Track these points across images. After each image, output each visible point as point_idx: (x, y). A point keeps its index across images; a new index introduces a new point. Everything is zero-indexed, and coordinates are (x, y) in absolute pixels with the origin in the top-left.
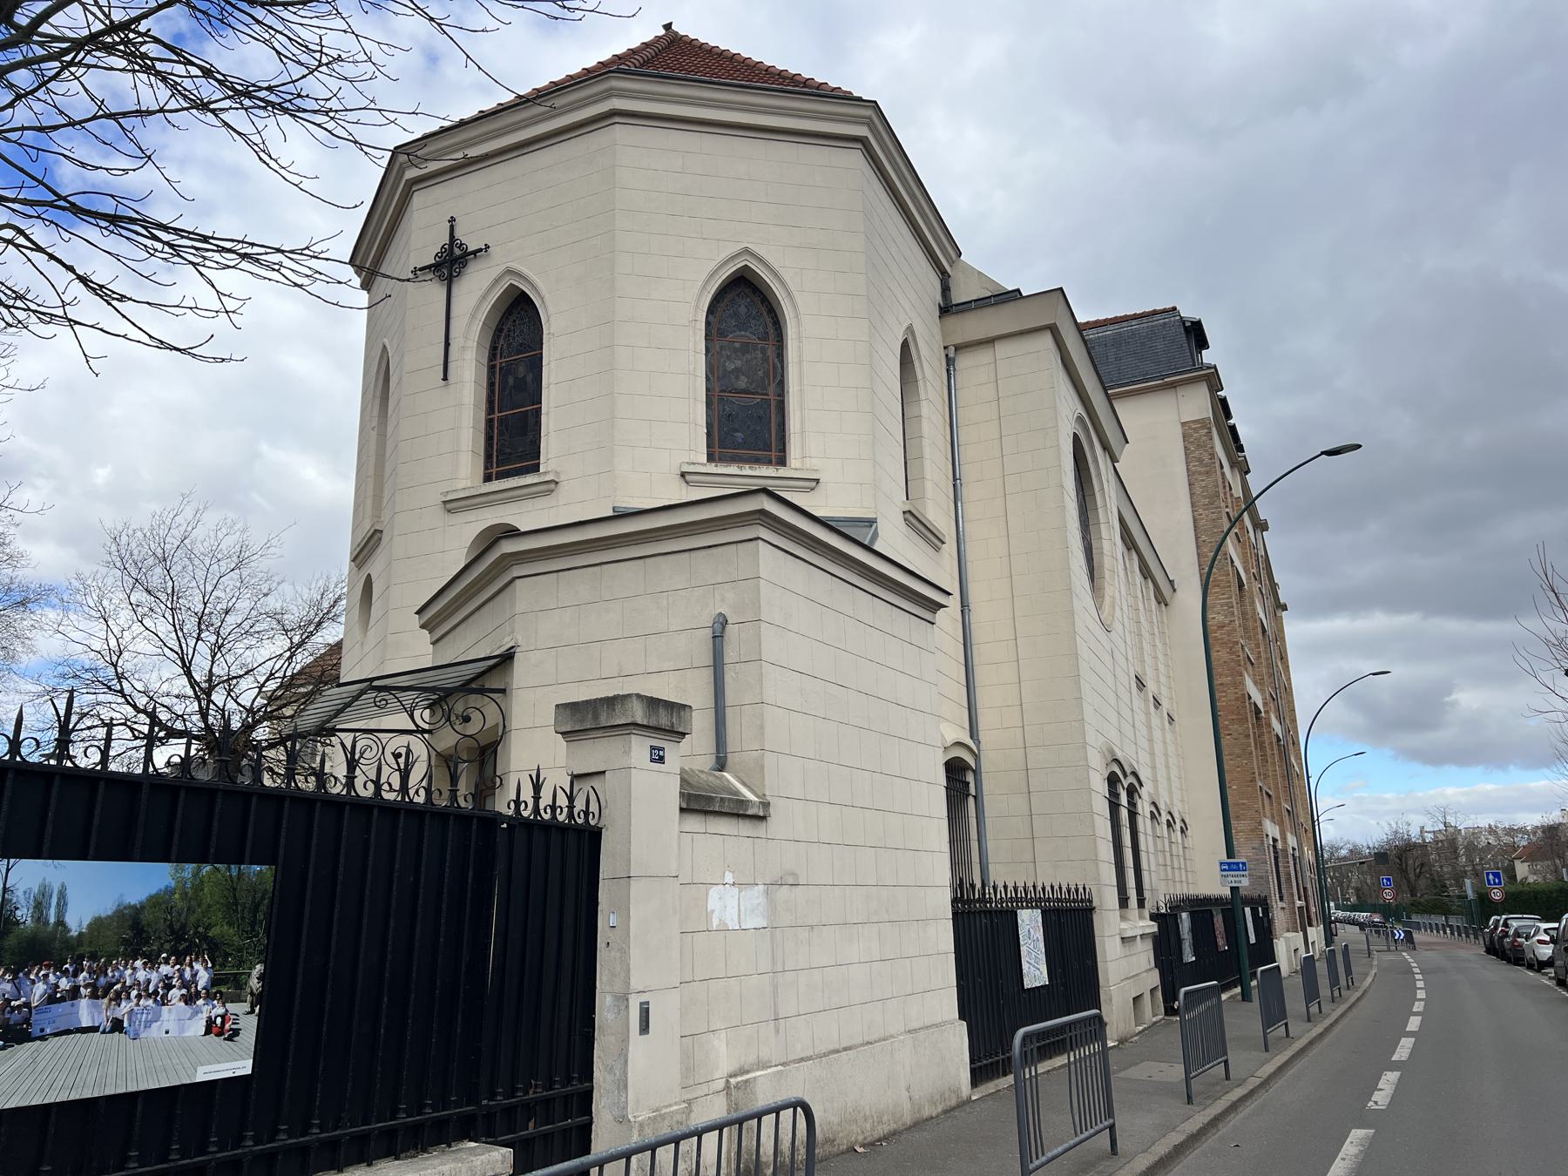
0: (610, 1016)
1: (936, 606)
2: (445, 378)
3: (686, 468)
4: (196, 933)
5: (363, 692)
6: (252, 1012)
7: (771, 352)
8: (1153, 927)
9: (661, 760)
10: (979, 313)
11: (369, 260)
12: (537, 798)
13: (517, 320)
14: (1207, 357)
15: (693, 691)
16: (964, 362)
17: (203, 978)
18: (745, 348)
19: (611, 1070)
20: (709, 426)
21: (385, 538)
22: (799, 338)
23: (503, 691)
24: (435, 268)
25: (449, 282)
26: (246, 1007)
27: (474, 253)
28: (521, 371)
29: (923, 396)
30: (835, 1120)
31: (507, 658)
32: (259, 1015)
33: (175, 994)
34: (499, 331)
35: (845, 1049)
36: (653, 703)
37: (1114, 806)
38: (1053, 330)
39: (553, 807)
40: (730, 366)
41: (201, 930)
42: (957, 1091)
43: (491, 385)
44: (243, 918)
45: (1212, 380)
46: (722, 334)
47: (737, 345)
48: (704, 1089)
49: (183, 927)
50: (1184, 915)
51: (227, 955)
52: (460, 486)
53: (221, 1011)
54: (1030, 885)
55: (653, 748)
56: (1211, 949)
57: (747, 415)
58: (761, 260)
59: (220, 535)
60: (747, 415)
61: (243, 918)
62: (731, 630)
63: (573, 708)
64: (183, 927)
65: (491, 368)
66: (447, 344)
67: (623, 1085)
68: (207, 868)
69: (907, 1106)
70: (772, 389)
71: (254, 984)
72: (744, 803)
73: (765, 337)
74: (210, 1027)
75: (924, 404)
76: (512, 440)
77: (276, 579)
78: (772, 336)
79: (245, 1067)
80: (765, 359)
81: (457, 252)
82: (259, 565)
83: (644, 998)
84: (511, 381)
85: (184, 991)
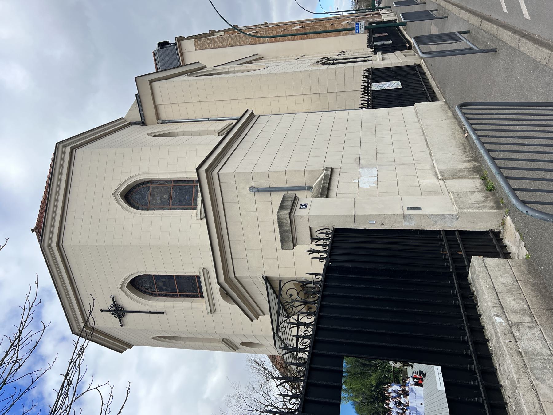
0: (413, 223)
1: (252, 114)
2: (163, 313)
3: (199, 218)
4: (374, 391)
5: (279, 338)
6: (412, 366)
7: (154, 185)
8: (379, 54)
9: (306, 205)
10: (144, 110)
11: (120, 345)
12: (319, 252)
13: (141, 285)
14: (172, 41)
15: (277, 198)
16: (164, 117)
17: (396, 387)
18: (153, 195)
19: (436, 222)
20: (182, 209)
21: (225, 337)
22: (149, 174)
23: (280, 281)
26: (409, 369)
27: (114, 302)
28: (160, 283)
29: (175, 131)
30: (455, 143)
31: (267, 279)
32: (413, 363)
33: (403, 400)
34: (145, 292)
35: (426, 141)
36: (282, 207)
37: (333, 64)
38: (151, 82)
39: (323, 246)
40: (159, 201)
41: (373, 389)
42: (442, 106)
43: (166, 296)
44: (368, 370)
45: (180, 39)
46: (147, 204)
47: (151, 198)
48: (444, 188)
49: (371, 397)
50: (375, 44)
51: (385, 377)
52: (204, 306)
53: (411, 380)
54: (362, 93)
55: (301, 208)
56: (387, 37)
57: (178, 194)
58: (118, 189)
59: (231, 405)
60: (178, 194)
61: (368, 370)
62: (256, 185)
63: (283, 241)
64: (371, 397)
65: (160, 295)
67: (442, 216)
68: (344, 386)
69: (448, 121)
70: (169, 185)
71: (399, 365)
72: (325, 176)
73: (149, 188)
74: (419, 384)
75: (178, 130)
76: (186, 287)
77: (248, 384)
78: (148, 185)
79: (437, 369)
80: (157, 187)
81: (114, 309)
82: (243, 391)
83: (405, 209)
84: (164, 288)
85: (402, 396)
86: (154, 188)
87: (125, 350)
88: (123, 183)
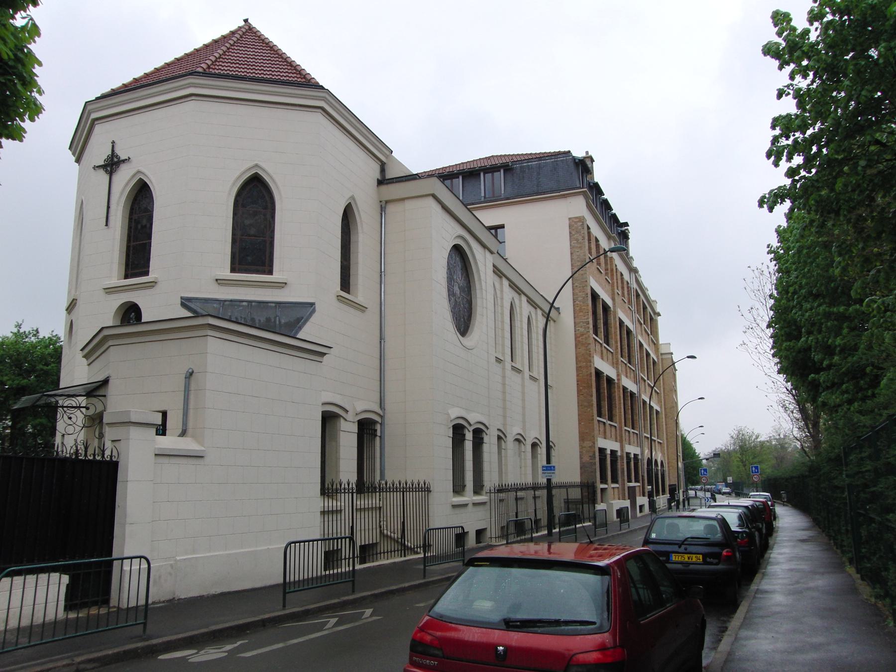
1: (323, 354)
2: (107, 225)
12: (86, 451)
23: (105, 396)
24: (103, 167)
25: (111, 174)
31: (105, 382)
38: (434, 196)
40: (247, 222)
43: (130, 228)
65: (130, 219)
66: (108, 207)
76: (137, 257)
81: (116, 160)
84: (139, 227)
86: (265, 215)
87: (74, 154)
88: (271, 177)
